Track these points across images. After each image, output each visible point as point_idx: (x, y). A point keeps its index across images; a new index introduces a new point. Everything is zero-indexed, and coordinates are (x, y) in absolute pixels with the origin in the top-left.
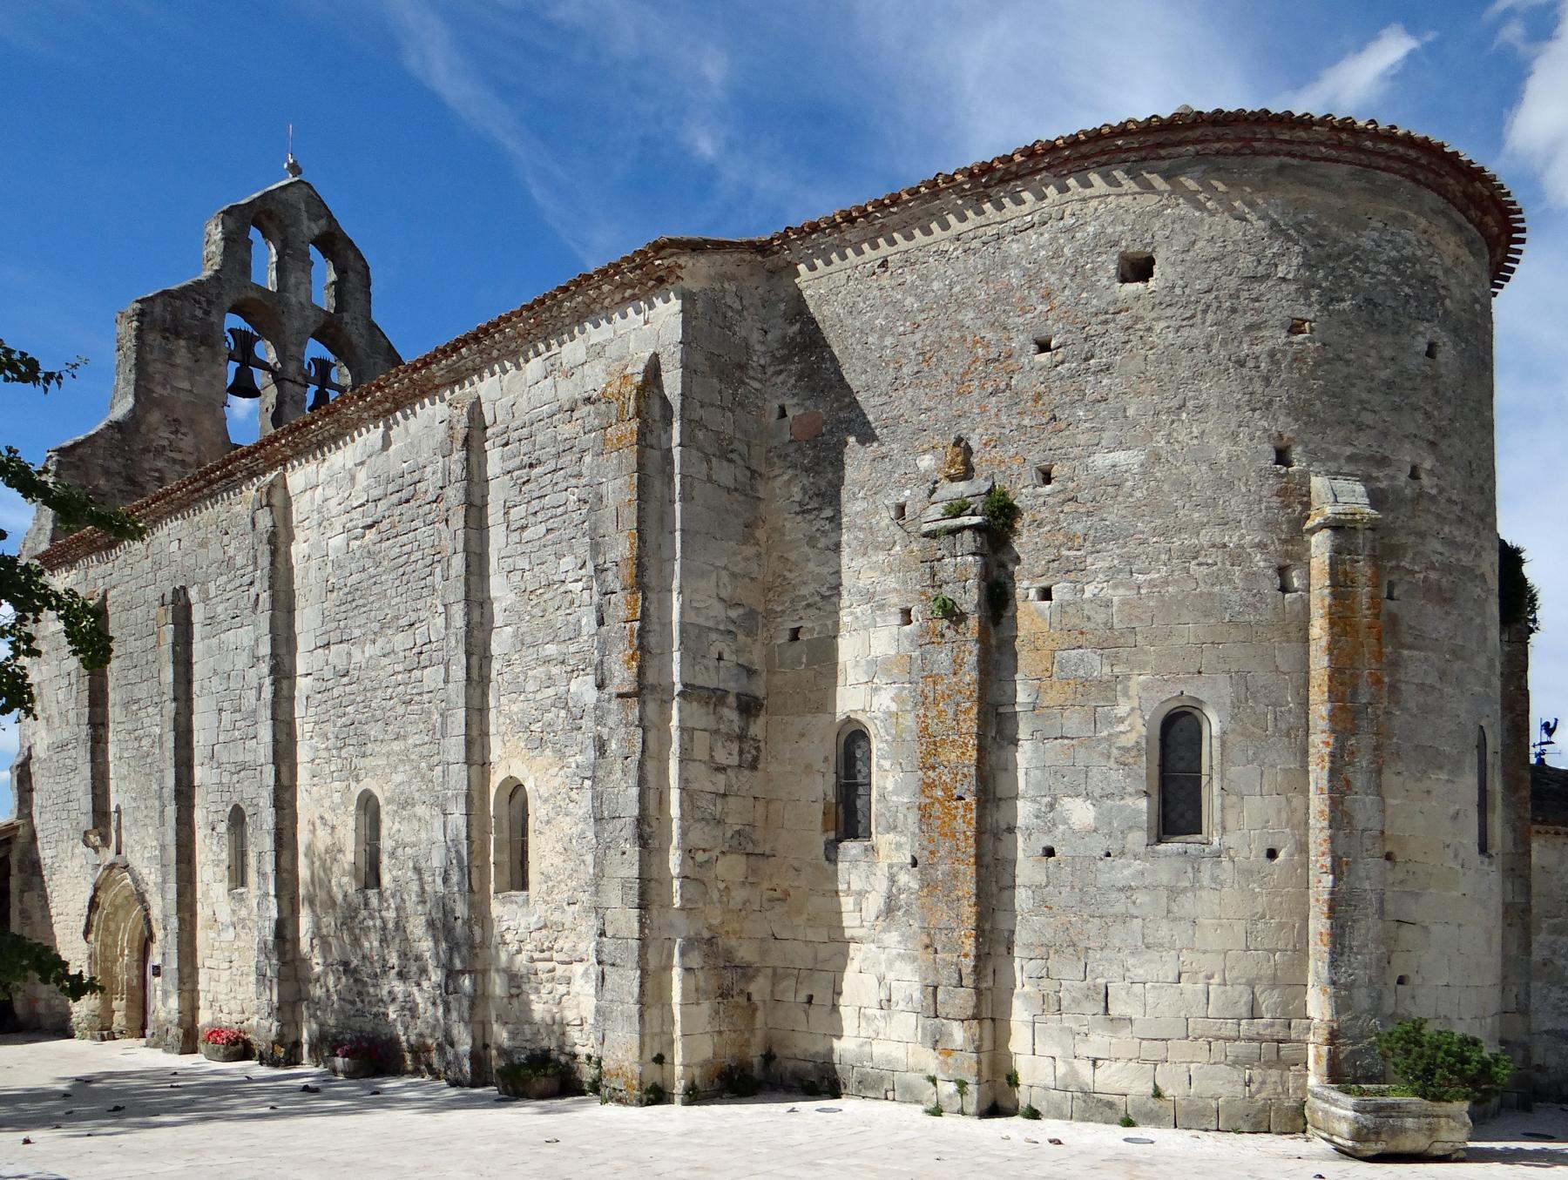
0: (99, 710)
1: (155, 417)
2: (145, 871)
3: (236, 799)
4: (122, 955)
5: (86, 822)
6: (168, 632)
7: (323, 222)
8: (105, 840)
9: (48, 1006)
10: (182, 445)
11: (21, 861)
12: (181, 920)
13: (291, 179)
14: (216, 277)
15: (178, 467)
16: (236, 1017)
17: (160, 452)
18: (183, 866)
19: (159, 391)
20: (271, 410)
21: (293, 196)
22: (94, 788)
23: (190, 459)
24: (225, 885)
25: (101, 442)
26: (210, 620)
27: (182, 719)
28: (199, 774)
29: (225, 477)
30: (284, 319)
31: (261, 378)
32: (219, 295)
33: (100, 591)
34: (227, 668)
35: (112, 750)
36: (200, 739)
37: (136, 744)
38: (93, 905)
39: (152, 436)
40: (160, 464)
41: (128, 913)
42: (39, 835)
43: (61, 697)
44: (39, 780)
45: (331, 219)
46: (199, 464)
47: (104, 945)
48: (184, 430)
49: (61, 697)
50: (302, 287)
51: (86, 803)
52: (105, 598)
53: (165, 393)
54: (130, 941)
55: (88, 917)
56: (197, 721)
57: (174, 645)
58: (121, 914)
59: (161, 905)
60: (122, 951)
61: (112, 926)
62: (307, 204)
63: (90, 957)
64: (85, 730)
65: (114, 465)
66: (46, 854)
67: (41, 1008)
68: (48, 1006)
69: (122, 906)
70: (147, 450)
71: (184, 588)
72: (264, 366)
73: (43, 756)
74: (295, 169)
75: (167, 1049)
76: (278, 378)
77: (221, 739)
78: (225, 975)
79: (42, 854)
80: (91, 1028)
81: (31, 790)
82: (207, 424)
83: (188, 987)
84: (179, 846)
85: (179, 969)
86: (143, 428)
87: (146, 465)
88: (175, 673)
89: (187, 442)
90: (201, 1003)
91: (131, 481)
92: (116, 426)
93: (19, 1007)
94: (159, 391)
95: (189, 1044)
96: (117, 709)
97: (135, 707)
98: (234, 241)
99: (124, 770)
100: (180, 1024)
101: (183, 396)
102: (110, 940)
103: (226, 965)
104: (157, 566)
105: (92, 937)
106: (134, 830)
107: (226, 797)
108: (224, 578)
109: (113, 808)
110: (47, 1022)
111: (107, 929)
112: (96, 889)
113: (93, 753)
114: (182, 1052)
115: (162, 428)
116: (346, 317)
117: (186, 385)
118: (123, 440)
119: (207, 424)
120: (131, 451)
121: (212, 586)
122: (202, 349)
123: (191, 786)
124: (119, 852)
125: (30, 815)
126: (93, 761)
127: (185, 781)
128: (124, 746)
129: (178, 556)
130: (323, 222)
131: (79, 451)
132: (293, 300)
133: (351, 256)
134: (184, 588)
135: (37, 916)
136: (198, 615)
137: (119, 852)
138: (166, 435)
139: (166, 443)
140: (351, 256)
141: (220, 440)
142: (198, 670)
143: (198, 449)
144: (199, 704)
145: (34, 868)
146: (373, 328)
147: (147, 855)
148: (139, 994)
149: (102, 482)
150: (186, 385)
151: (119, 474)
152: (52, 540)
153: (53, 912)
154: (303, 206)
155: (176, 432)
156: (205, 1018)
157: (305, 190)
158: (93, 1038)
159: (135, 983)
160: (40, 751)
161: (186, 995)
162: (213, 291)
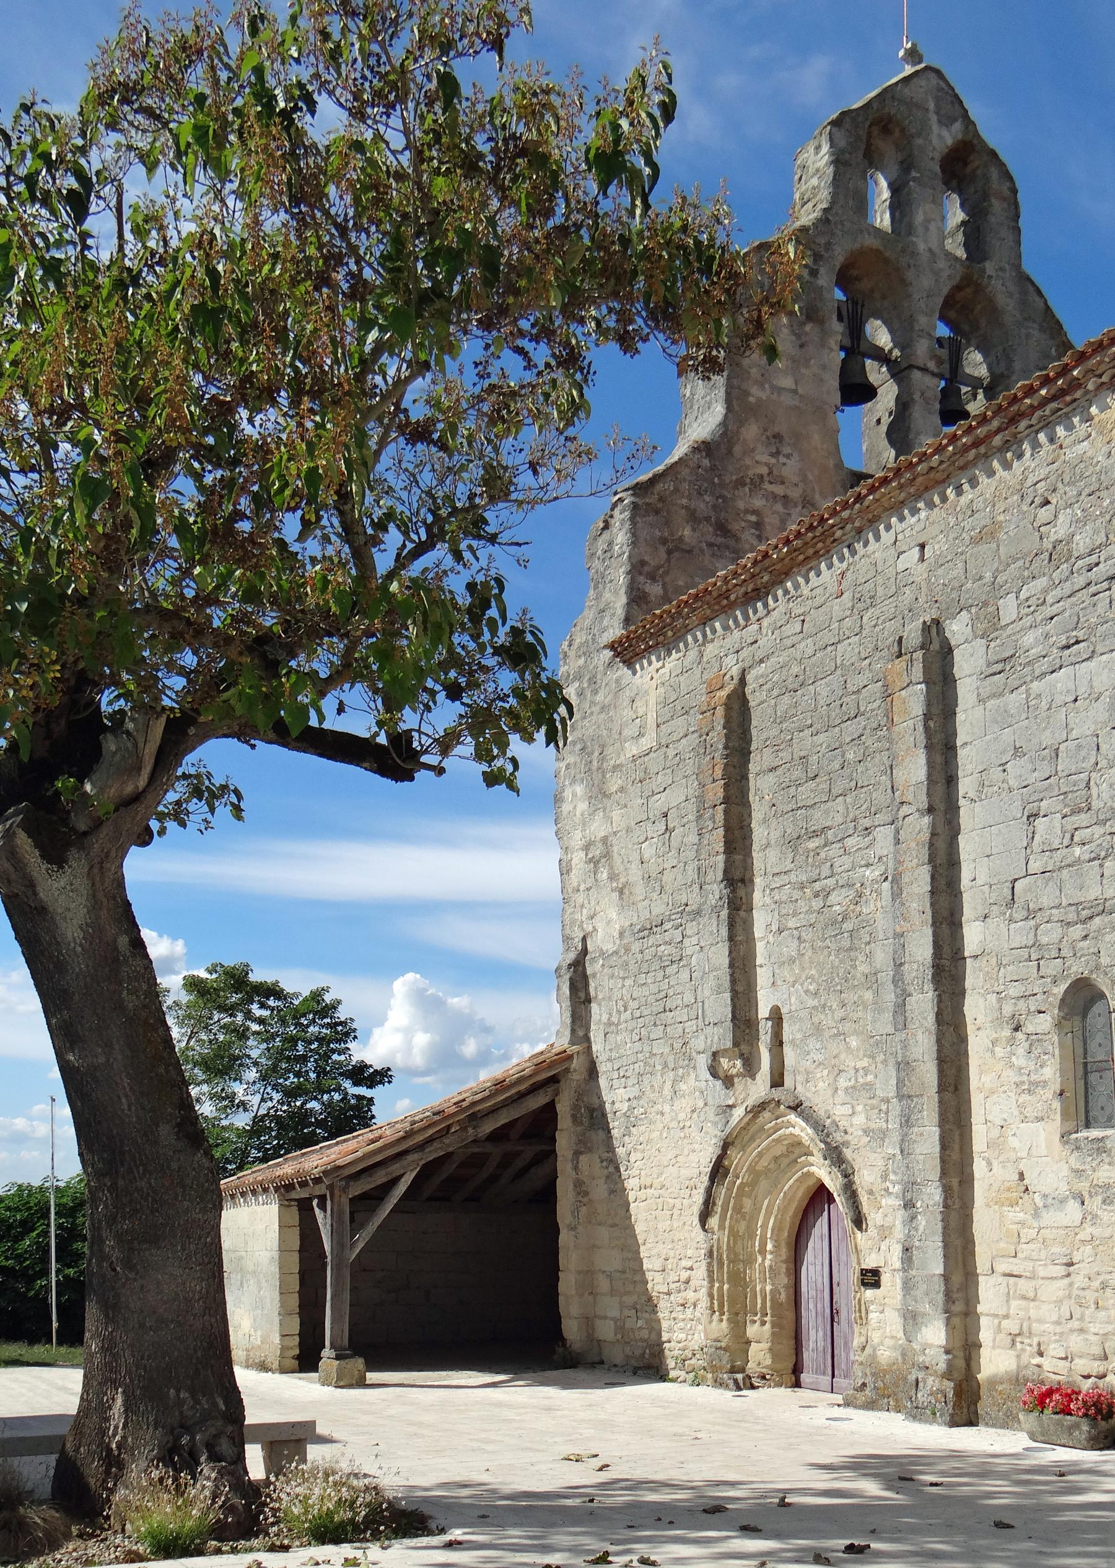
0: (738, 857)
1: (751, 432)
2: (840, 1112)
3: (1078, 969)
4: (763, 1251)
5: (721, 1036)
6: (913, 701)
7: (958, 126)
8: (750, 1067)
9: (620, 1328)
10: (786, 472)
11: (575, 1107)
12: (947, 1190)
13: (909, 70)
14: (825, 220)
15: (779, 507)
16: (1083, 1365)
17: (756, 483)
18: (948, 1096)
19: (757, 393)
20: (886, 420)
21: (921, 90)
22: (733, 981)
23: (795, 494)
24: (1055, 1124)
25: (685, 472)
26: (1001, 665)
27: (941, 844)
28: (973, 935)
29: (1054, 398)
30: (910, 275)
31: (876, 373)
32: (828, 246)
33: (735, 671)
34: (1047, 738)
35: (761, 921)
36: (974, 872)
37: (817, 904)
38: (718, 1171)
39: (748, 461)
40: (758, 503)
41: (776, 1184)
42: (602, 1068)
43: (648, 850)
44: (601, 983)
45: (969, 123)
46: (807, 503)
47: (734, 1234)
48: (786, 450)
49: (648, 850)
50: (932, 227)
51: (720, 1006)
52: (743, 682)
53: (763, 396)
54: (777, 1229)
55: (709, 1192)
56: (967, 846)
57: (927, 717)
58: (764, 1184)
59: (888, 1170)
60: (763, 1245)
61: (747, 1203)
62: (937, 100)
63: (710, 1254)
64: (716, 891)
65: (702, 506)
66: (615, 1095)
67: (606, 1331)
68: (620, 1328)
69: (767, 1171)
70: (741, 483)
71: (937, 622)
72: (881, 356)
73: (609, 947)
74: (913, 55)
75: (917, 1413)
76: (898, 371)
77: (1035, 866)
78: (1055, 1290)
79: (607, 1097)
80: (714, 1369)
81: (588, 1000)
82: (816, 438)
83: (958, 1307)
84: (942, 1061)
85: (946, 1277)
86: (737, 449)
87: (741, 505)
88: (930, 764)
89: (790, 468)
90: (985, 1335)
91: (722, 528)
92: (704, 448)
93: (571, 1329)
94: (757, 393)
95: (965, 1404)
96: (773, 855)
97: (812, 844)
98: (846, 164)
99: (790, 948)
100: (948, 1375)
101: (787, 400)
102: (742, 1227)
103: (1061, 1270)
104: (864, 602)
105: (713, 1222)
106: (812, 1044)
107: (1051, 968)
108: (1042, 582)
109: (763, 1011)
110: (617, 1355)
111: (738, 1209)
112: (726, 1145)
113: (731, 925)
114: (954, 1423)
115: (760, 448)
116: (990, 267)
117: (787, 382)
118: (713, 468)
119: (816, 438)
120: (722, 485)
121: (1009, 608)
122: (808, 328)
123: (958, 957)
124: (777, 1081)
125: (587, 1039)
126: (731, 938)
127: (947, 951)
128: (788, 909)
129: (920, 572)
130: (958, 126)
131: (659, 487)
132: (922, 247)
133: (994, 174)
134: (937, 622)
135: (599, 1190)
136: (968, 664)
137: (777, 1081)
138: (764, 458)
139: (764, 470)
140: (994, 174)
141: (831, 463)
142: (968, 760)
143: (804, 479)
144: (970, 815)
145: (595, 1118)
146: (1025, 280)
147: (843, 1083)
148: (791, 1315)
149: (687, 532)
150: (787, 382)
151: (707, 519)
152: (627, 621)
153: (630, 1184)
154: (932, 106)
155: (776, 454)
156: (994, 1362)
157: (934, 80)
158: (719, 1384)
159: (783, 1297)
160: (604, 940)
161: (956, 1321)
162: (822, 240)
